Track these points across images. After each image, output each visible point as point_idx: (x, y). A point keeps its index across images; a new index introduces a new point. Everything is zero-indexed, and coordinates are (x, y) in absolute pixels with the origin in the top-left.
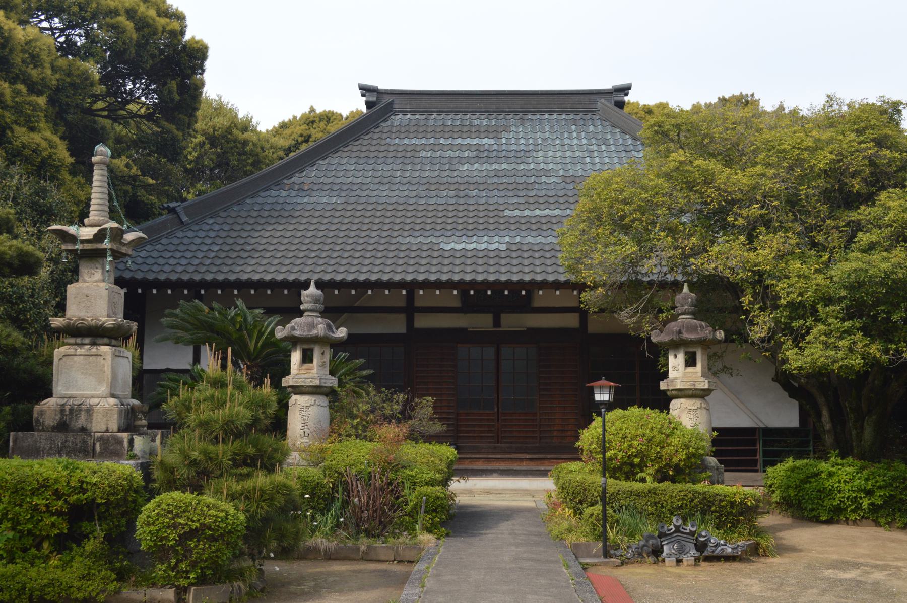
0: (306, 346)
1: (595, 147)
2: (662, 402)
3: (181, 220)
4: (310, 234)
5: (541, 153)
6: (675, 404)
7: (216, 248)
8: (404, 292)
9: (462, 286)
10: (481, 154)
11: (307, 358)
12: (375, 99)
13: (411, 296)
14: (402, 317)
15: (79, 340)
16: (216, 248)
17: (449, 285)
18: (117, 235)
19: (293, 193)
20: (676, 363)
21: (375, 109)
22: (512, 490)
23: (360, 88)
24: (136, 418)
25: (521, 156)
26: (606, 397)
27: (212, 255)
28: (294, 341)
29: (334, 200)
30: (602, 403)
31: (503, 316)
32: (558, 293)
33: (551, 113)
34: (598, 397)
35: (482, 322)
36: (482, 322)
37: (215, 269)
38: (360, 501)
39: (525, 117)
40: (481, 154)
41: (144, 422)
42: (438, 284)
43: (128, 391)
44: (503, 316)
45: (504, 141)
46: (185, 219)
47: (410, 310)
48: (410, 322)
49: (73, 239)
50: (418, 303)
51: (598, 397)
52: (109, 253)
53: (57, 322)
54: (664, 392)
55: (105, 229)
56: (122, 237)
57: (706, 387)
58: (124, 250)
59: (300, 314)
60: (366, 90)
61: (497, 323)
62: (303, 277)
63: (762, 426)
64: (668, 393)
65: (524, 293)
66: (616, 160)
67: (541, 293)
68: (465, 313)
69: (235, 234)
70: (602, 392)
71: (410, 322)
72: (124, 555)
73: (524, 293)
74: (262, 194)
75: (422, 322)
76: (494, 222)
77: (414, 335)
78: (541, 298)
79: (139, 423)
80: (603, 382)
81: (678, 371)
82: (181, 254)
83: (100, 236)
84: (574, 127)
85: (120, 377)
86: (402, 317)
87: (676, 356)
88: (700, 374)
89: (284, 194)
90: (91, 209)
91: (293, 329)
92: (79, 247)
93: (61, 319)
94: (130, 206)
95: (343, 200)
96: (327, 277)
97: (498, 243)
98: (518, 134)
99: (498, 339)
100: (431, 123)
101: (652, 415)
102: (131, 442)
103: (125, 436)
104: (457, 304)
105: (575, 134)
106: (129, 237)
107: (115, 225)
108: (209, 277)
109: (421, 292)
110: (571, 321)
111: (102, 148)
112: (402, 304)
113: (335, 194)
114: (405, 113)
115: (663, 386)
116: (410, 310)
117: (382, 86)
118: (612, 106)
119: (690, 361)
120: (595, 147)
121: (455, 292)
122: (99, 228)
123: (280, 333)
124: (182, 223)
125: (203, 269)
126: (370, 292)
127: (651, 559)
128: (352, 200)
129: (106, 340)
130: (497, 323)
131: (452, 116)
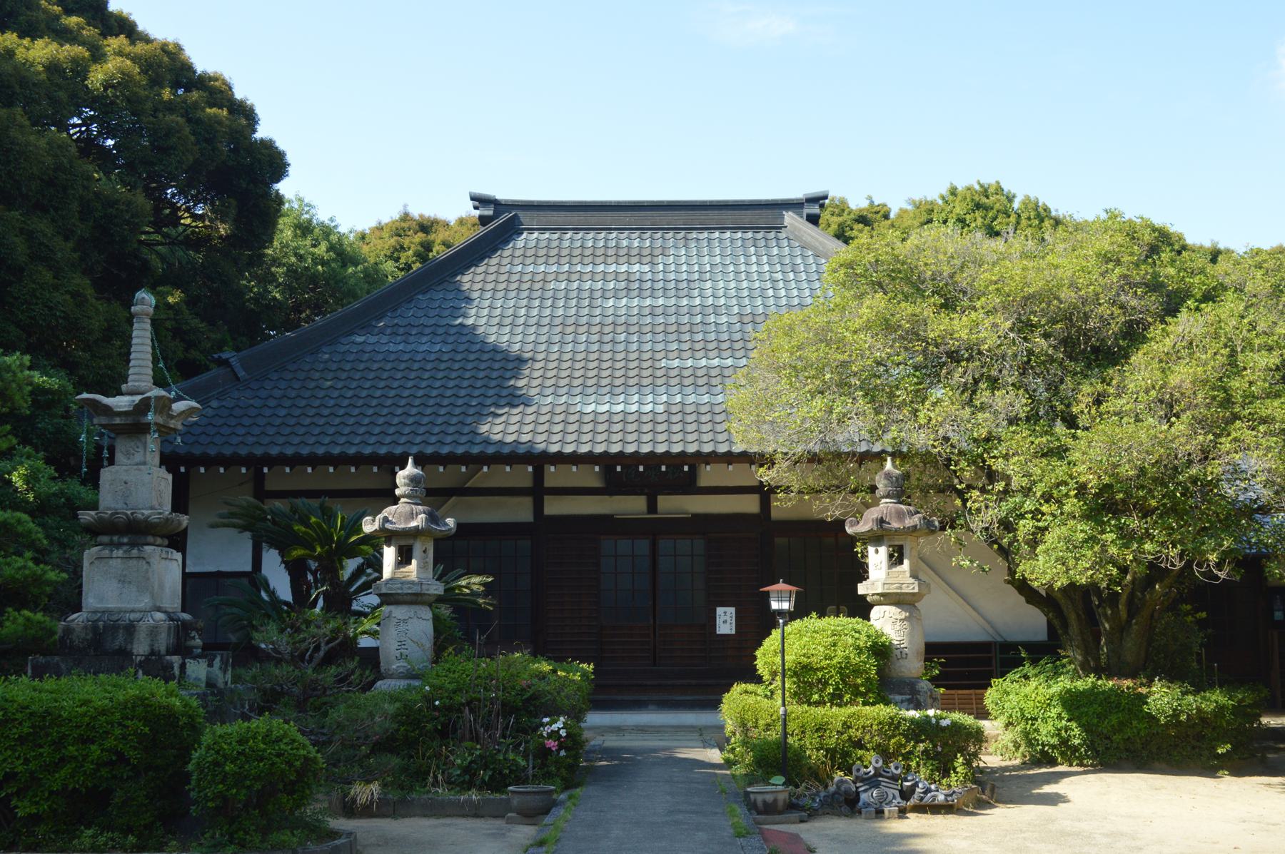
0: (403, 543)
1: (779, 276)
2: (862, 608)
3: (235, 374)
4: (406, 393)
5: (709, 284)
6: (876, 612)
7: (283, 412)
8: (530, 469)
9: (606, 460)
10: (632, 286)
11: (404, 557)
12: (491, 213)
13: (539, 475)
14: (527, 502)
15: (115, 538)
16: (283, 412)
17: (590, 458)
18: (164, 406)
19: (384, 339)
20: (877, 558)
21: (492, 226)
22: (673, 727)
23: (472, 199)
24: (188, 637)
25: (683, 288)
26: (785, 606)
27: (278, 421)
28: (388, 536)
29: (437, 347)
30: (780, 613)
31: (660, 499)
32: (731, 467)
33: (723, 230)
34: (775, 605)
35: (633, 505)
36: (633, 505)
37: (281, 440)
38: (75, 126)
39: (690, 236)
40: (632, 286)
41: (198, 642)
42: (575, 458)
43: (177, 604)
44: (660, 499)
45: (661, 267)
46: (241, 374)
47: (538, 491)
48: (538, 507)
49: (107, 410)
50: (549, 482)
51: (775, 605)
52: (153, 428)
53: (86, 516)
54: (864, 597)
55: (149, 398)
56: (170, 408)
57: (916, 590)
58: (172, 424)
59: (395, 501)
60: (480, 201)
61: (652, 507)
62: (398, 450)
63: (999, 639)
64: (868, 599)
65: (686, 468)
66: (807, 293)
67: (708, 468)
68: (611, 494)
69: (308, 394)
70: (780, 600)
71: (538, 507)
72: (171, 809)
73: (686, 468)
74: (343, 340)
75: (553, 507)
76: (647, 376)
77: (543, 526)
78: (709, 475)
79: (192, 643)
80: (781, 586)
81: (880, 573)
82: (255, 439)
83: (143, 407)
84: (753, 249)
85: (917, 841)
86: (527, 502)
87: (877, 552)
88: (908, 574)
89: (373, 339)
90: (131, 371)
91: (386, 520)
92: (117, 421)
93: (93, 513)
94: (179, 364)
95: (449, 347)
96: (429, 450)
97: (651, 404)
98: (682, 256)
99: (654, 529)
100: (566, 244)
101: (856, 622)
102: (183, 667)
103: (176, 660)
104: (596, 483)
105: (754, 259)
106: (179, 407)
107: (162, 393)
108: (274, 451)
109: (552, 469)
110: (750, 504)
111: (144, 295)
112: (527, 483)
113: (439, 339)
114: (531, 230)
115: (862, 589)
116: (538, 491)
117: (502, 194)
118: (803, 221)
119: (896, 557)
120: (779, 276)
121: (597, 469)
122: (137, 398)
123: (369, 526)
124: (238, 379)
125: (266, 440)
126: (485, 469)
127: (845, 809)
128: (462, 348)
129: (150, 539)
130: (652, 507)
131: (592, 235)
